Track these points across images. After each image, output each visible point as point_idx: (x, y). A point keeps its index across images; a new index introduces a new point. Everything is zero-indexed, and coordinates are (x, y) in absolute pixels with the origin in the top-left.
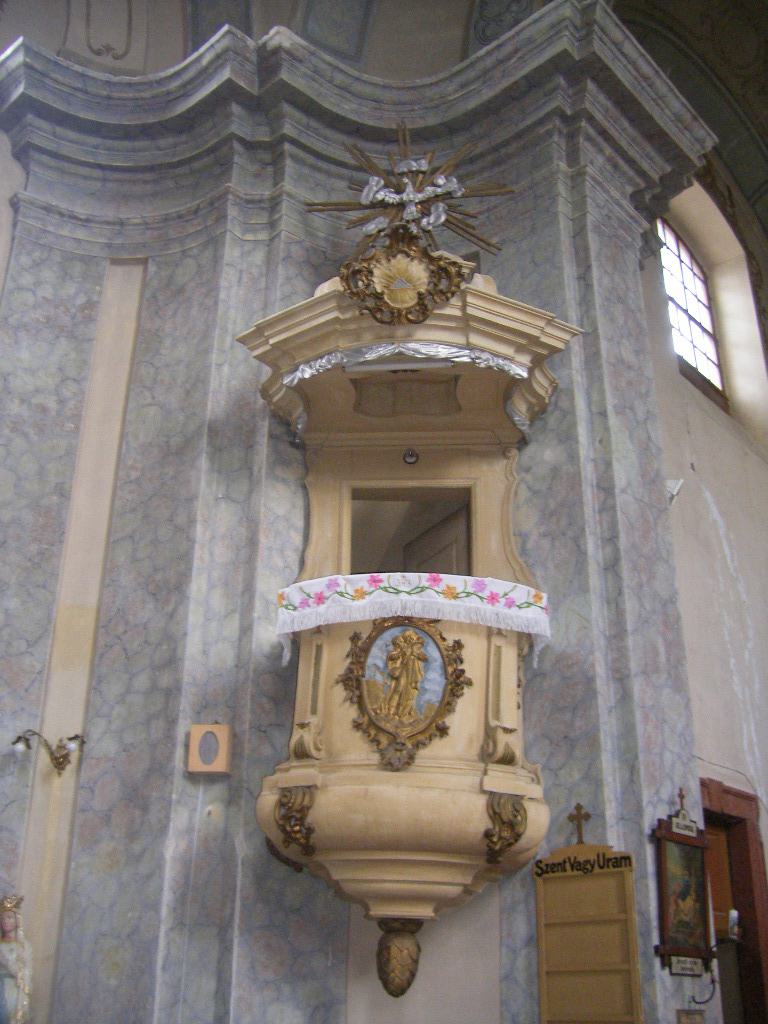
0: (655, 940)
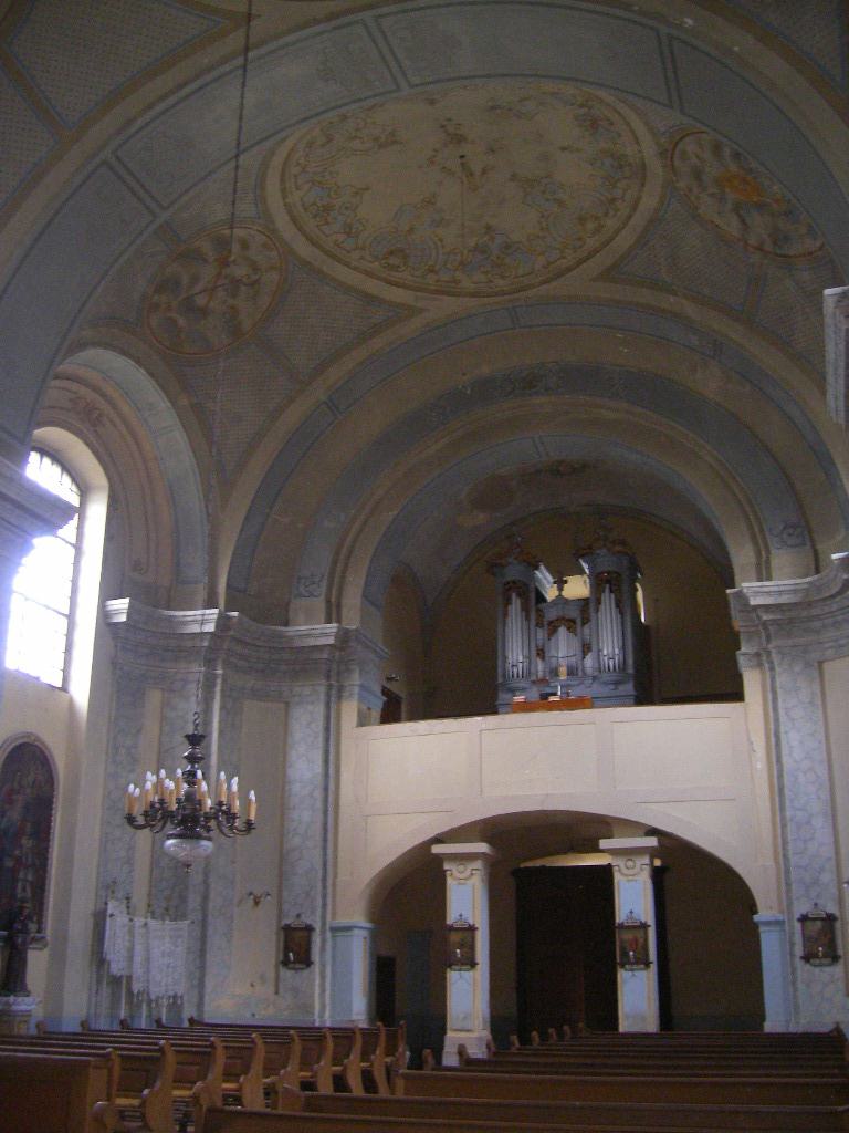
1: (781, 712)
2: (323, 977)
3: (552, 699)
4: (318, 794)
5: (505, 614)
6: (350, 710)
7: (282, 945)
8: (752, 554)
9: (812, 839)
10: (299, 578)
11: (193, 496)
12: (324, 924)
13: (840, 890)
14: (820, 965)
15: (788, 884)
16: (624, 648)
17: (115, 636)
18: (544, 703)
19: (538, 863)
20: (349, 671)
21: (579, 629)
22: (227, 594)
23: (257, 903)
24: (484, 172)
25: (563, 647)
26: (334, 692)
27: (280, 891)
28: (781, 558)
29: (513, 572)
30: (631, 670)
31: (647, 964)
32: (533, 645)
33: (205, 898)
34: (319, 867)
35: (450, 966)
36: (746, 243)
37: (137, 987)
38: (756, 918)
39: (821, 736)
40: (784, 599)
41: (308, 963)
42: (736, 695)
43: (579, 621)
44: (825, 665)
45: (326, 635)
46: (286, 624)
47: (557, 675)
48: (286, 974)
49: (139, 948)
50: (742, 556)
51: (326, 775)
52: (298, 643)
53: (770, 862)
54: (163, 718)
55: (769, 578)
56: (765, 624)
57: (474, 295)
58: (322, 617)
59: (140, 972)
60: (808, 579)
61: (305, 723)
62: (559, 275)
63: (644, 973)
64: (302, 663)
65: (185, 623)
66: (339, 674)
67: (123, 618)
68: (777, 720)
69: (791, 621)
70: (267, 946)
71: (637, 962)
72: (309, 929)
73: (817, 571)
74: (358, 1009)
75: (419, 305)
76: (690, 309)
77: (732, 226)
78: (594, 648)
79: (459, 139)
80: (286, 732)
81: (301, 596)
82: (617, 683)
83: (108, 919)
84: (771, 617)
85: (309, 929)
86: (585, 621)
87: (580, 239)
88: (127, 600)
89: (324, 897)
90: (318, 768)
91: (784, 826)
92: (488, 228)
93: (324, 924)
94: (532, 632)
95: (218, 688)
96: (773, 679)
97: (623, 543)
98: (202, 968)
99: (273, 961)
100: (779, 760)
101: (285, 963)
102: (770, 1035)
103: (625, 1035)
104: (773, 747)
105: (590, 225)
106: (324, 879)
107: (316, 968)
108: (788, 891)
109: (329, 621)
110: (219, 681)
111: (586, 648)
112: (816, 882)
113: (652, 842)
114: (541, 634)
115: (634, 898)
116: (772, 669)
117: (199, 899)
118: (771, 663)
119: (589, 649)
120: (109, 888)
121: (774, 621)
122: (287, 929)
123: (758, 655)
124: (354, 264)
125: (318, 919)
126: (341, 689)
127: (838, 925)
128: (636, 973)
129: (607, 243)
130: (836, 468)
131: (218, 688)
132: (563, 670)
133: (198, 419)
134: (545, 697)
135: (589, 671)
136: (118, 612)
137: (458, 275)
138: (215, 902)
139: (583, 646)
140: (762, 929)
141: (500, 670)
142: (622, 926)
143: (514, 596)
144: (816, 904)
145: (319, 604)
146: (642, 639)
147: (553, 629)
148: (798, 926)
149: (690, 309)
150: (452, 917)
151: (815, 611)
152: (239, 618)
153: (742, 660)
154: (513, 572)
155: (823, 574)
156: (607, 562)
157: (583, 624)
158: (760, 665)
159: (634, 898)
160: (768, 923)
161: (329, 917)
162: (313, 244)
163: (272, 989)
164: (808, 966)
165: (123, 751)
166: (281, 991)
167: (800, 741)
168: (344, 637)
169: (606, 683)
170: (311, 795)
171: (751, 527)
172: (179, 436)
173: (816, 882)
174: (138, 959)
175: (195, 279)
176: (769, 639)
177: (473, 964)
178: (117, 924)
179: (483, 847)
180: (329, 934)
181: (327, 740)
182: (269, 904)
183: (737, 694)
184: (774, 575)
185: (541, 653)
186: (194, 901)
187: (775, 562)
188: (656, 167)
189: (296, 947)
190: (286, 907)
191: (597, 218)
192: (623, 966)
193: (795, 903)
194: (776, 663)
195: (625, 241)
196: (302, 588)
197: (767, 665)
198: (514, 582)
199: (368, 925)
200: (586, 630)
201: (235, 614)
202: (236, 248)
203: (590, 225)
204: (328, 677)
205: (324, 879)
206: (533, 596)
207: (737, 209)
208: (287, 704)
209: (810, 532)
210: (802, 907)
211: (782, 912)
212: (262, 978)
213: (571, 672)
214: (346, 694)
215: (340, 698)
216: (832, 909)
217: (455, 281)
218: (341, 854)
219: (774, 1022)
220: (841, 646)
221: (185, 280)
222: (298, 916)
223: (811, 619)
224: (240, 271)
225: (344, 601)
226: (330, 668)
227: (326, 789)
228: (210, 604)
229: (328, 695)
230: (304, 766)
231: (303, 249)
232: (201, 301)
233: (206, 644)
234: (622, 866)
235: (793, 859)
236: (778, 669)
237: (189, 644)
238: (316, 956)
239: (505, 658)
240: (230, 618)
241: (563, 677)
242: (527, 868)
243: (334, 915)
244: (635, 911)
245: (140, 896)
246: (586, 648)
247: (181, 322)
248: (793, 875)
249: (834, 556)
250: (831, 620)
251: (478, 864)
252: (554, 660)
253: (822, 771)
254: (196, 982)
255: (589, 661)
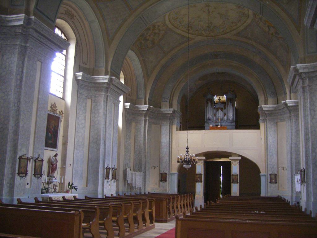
0: (105, 177)
1: (268, 132)
2: (169, 184)
3: (218, 126)
4: (168, 145)
5: (207, 106)
6: (174, 127)
7: (160, 177)
8: (264, 98)
9: (273, 159)
10: (163, 97)
11: (141, 79)
12: (169, 173)
13: (278, 170)
14: (273, 184)
15: (267, 168)
16: (233, 115)
17: (78, 84)
18: (216, 127)
19: (211, 160)
20: (175, 118)
21: (223, 110)
22: (149, 101)
23: (155, 168)
24: (213, 12)
25: (220, 114)
26: (171, 123)
27: (160, 166)
28: (270, 100)
29: (209, 97)
30: (234, 120)
31: (238, 183)
32: (213, 114)
33: (145, 168)
34: (168, 161)
35: (196, 182)
36: (269, 33)
37: (133, 185)
38: (260, 174)
39: (276, 138)
40: (270, 109)
41: (166, 181)
42: (257, 127)
43: (223, 109)
44: (278, 123)
45: (170, 111)
46: (160, 108)
47: (218, 120)
48: (161, 183)
49: (134, 178)
50: (261, 98)
51: (170, 141)
52: (164, 112)
53: (264, 163)
54: (135, 129)
55: (267, 104)
56: (266, 114)
57: (206, 36)
58: (169, 107)
59: (134, 183)
60: (276, 105)
61: (165, 130)
62: (225, 34)
63: (237, 184)
64: (165, 117)
65: (140, 108)
66: (172, 119)
67: (128, 107)
68: (267, 134)
69: (272, 113)
70: (157, 178)
71: (236, 182)
72: (166, 174)
73: (278, 104)
74: (175, 190)
75: (193, 38)
76: (254, 44)
77: (267, 29)
78: (227, 114)
79: (208, 6)
80: (160, 133)
81: (163, 101)
82: (231, 123)
83: (127, 172)
84: (268, 112)
85: (166, 174)
86: (225, 108)
87: (232, 26)
88: (129, 103)
89: (169, 167)
90: (168, 140)
91: (267, 156)
92: (211, 22)
93: (169, 173)
94: (213, 110)
95: (147, 122)
96: (267, 126)
97: (233, 91)
98: (145, 181)
99: (158, 180)
100: (267, 143)
101: (161, 181)
102: (263, 197)
103: (232, 196)
104: (266, 139)
105: (234, 24)
106: (169, 163)
107: (168, 182)
108: (267, 169)
109: (170, 108)
110: (147, 121)
111: (225, 115)
112: (273, 167)
113: (240, 158)
114: (215, 111)
115: (235, 169)
116: (267, 123)
117: (144, 168)
118: (266, 122)
119: (225, 115)
120: (126, 165)
121: (268, 113)
122: (161, 174)
123: (264, 120)
124: (180, 29)
125: (168, 172)
126: (173, 123)
127: (277, 176)
128: (236, 184)
129: (238, 28)
130: (284, 82)
131: (147, 122)
132: (220, 119)
133: (144, 63)
134: (217, 126)
135: (225, 119)
136: (127, 106)
137: (203, 32)
138: (147, 168)
139: (224, 114)
140: (261, 176)
141: (205, 119)
142: (233, 175)
143: (209, 102)
144: (273, 172)
145: (168, 104)
146: (237, 112)
147: (218, 109)
148: (269, 176)
149: (254, 44)
150: (197, 172)
151: (277, 112)
152: (153, 108)
153: (260, 121)
154: (209, 97)
155: (279, 104)
156: (230, 96)
157: (224, 109)
158: (264, 122)
159: (235, 169)
160: (263, 175)
161: (170, 172)
162: (172, 25)
163: (158, 186)
164: (270, 184)
165: (128, 136)
166: (160, 186)
167: (272, 139)
168: (174, 112)
169: (229, 123)
170: (166, 146)
171: (264, 93)
172: (139, 66)
173: (273, 167)
174: (134, 180)
175: (147, 34)
176: (266, 117)
177: (201, 182)
178: (129, 173)
179: (204, 158)
180: (170, 175)
181: (170, 134)
182: (157, 170)
183: (256, 125)
184: (268, 104)
185: (215, 115)
186: (143, 168)
187: (269, 100)
188: (251, 16)
189: (163, 178)
190: (161, 169)
191: (236, 23)
192: (233, 183)
193: (269, 171)
194: (267, 122)
195: (242, 28)
196: (164, 100)
197: (266, 122)
198: (209, 99)
199: (177, 173)
200: (225, 110)
201: (152, 106)
202: (157, 27)
203: (234, 24)
204: (170, 120)
205: (169, 163)
206: (213, 102)
207: (268, 26)
208: (161, 125)
209: (277, 95)
210: (270, 172)
211: (266, 173)
212: (156, 184)
213: (221, 120)
214: (174, 123)
215: (172, 125)
216: (276, 173)
217: (202, 33)
218: (173, 158)
219: (263, 194)
220: (281, 120)
221: (146, 33)
222: (164, 171)
223: (275, 113)
224: (157, 31)
225: (173, 103)
226: (170, 118)
227: (169, 144)
228: (145, 104)
229: (170, 124)
230: (165, 139)
231: (170, 26)
232: (148, 38)
233: (145, 113)
234: (233, 163)
235: (269, 163)
236: (268, 123)
237: (141, 112)
238: (167, 179)
239: (207, 116)
240: (150, 107)
241: (220, 121)
242: (209, 161)
243: (171, 171)
244: (236, 172)
245: (132, 168)
246: (225, 115)
247: (143, 42)
248: (269, 165)
249: (282, 102)
250: (280, 114)
251: (203, 161)
252: (217, 117)
253: (276, 145)
254: (144, 185)
255: (225, 117)
